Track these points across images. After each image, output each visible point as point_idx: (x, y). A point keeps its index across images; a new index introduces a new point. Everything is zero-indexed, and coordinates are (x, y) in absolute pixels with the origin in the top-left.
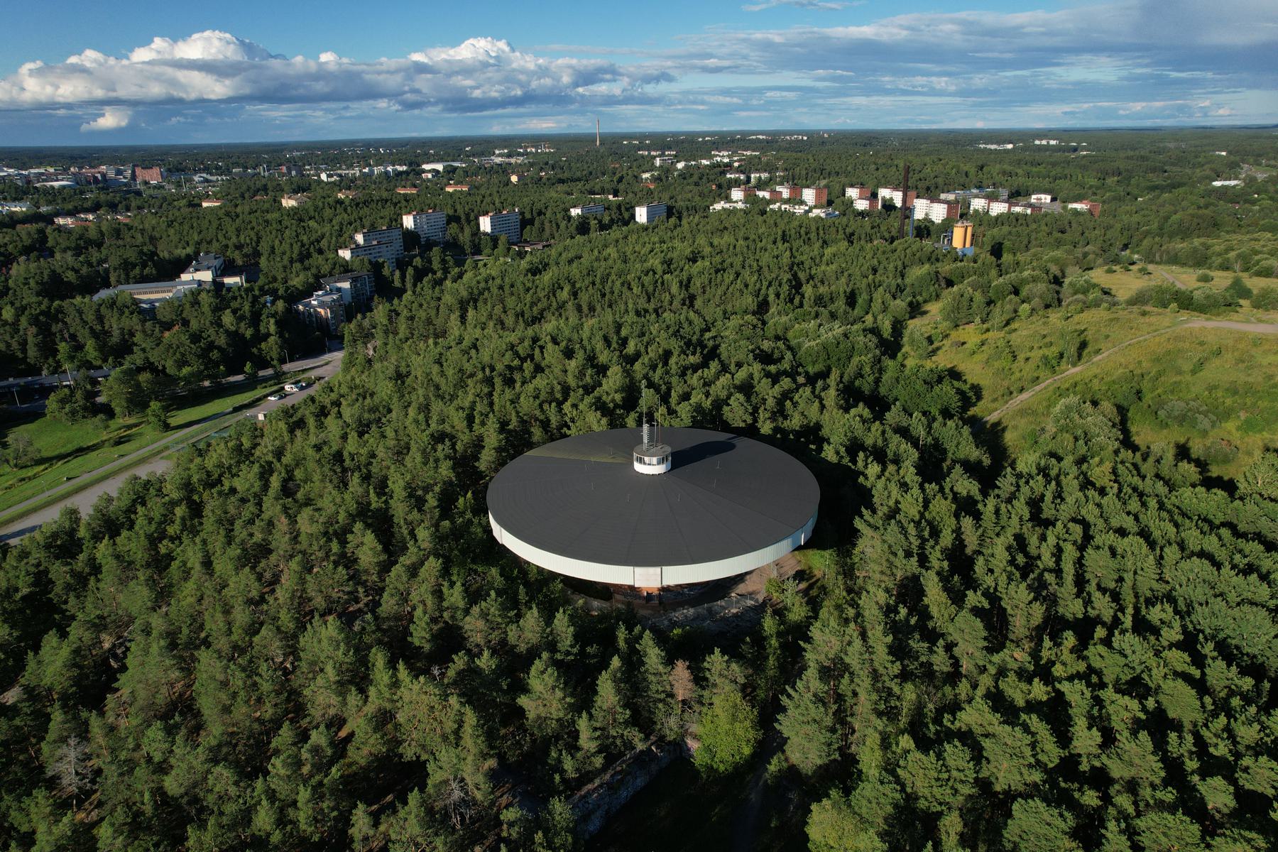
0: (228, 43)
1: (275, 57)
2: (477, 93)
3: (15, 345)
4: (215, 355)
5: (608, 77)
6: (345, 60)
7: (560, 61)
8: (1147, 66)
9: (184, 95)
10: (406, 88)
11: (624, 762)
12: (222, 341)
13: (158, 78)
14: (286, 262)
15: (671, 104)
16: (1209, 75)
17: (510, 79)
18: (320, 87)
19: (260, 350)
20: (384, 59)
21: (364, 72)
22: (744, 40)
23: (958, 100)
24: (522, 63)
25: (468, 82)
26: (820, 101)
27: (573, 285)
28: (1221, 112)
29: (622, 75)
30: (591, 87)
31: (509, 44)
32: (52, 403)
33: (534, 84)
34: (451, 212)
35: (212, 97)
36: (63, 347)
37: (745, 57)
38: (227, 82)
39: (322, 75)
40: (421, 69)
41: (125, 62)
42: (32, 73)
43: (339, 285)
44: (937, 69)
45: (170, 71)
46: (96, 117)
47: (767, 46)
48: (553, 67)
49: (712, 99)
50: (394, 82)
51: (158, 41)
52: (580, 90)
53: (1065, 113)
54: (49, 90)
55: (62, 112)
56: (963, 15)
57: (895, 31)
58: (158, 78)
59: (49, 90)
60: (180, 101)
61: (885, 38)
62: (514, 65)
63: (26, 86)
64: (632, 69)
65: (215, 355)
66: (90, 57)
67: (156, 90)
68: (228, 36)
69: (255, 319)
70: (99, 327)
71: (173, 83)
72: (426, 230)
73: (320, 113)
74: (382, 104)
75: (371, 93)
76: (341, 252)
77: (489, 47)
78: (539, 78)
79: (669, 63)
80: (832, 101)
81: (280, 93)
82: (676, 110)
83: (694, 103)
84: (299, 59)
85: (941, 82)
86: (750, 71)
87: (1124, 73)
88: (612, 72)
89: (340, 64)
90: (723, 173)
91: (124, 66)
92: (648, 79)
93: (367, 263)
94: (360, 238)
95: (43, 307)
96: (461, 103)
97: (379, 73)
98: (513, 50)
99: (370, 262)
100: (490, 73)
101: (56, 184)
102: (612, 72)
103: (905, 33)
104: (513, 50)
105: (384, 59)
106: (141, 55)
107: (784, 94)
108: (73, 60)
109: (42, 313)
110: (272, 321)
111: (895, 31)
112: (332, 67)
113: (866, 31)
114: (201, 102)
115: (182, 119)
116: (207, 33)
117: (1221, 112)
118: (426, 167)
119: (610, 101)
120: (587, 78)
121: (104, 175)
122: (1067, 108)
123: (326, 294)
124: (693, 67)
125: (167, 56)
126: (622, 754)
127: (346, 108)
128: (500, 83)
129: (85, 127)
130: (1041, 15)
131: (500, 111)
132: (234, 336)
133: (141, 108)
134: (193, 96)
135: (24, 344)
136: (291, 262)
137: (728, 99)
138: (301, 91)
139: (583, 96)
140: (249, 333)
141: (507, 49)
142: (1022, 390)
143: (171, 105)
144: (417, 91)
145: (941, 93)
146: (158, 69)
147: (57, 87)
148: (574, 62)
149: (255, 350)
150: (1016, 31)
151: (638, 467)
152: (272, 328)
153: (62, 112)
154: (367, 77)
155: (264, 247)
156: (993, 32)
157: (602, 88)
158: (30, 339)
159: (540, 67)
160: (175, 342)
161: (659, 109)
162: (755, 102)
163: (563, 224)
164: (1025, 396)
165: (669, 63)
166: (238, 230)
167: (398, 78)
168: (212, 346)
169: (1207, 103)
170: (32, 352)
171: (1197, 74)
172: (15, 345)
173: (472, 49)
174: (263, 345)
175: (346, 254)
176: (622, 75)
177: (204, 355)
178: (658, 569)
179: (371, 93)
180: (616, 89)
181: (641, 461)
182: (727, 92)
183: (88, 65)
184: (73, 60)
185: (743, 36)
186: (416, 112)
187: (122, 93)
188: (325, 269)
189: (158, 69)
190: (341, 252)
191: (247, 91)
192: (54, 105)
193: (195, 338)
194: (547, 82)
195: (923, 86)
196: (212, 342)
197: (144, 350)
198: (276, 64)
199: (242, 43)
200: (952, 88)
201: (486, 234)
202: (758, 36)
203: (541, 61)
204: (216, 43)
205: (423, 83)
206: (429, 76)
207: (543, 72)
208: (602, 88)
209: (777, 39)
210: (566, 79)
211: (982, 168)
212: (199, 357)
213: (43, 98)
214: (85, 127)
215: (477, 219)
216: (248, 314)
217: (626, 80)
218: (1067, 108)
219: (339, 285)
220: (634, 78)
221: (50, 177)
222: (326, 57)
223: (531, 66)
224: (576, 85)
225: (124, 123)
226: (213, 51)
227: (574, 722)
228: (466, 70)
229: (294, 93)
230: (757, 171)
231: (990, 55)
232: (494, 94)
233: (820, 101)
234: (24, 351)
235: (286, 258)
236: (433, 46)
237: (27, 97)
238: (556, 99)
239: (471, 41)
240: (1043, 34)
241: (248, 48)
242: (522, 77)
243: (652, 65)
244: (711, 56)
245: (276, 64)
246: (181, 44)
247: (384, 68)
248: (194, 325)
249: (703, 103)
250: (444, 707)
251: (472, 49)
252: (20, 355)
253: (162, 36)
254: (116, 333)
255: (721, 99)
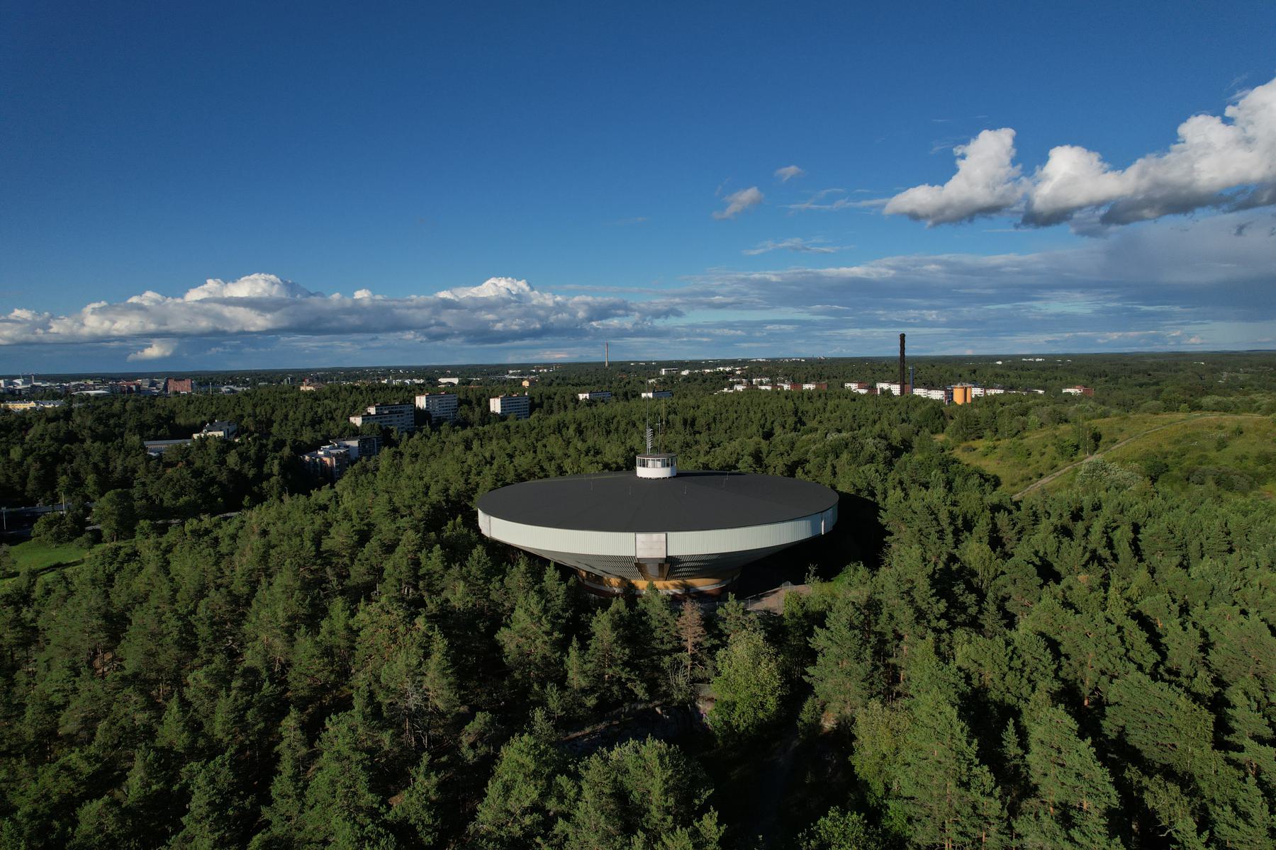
0: (273, 284)
1: (314, 295)
2: (499, 326)
3: (15, 478)
4: (214, 490)
5: (620, 312)
6: (379, 297)
7: (577, 299)
8: (1117, 300)
9: (227, 328)
10: (433, 322)
11: (617, 717)
12: (223, 477)
13: (206, 314)
14: (297, 426)
15: (679, 335)
16: (1177, 309)
17: (529, 314)
18: (354, 320)
19: (261, 488)
20: (414, 297)
21: (394, 306)
22: (744, 280)
23: (946, 330)
24: (541, 300)
25: (491, 317)
26: (818, 333)
27: (580, 424)
28: (1193, 340)
29: (632, 310)
30: (604, 322)
31: (529, 284)
32: (38, 527)
33: (552, 318)
34: (462, 397)
35: (253, 329)
36: (63, 480)
37: (745, 294)
38: (269, 316)
39: (357, 309)
40: (447, 304)
41: (179, 301)
42: (94, 312)
43: (348, 443)
44: (926, 303)
45: (217, 307)
46: (142, 348)
47: (765, 284)
48: (570, 303)
49: (718, 332)
50: (421, 316)
51: (210, 282)
52: (594, 324)
53: (1048, 342)
54: (107, 324)
55: (115, 344)
56: (945, 257)
57: (883, 270)
58: (206, 314)
59: (107, 324)
60: (224, 333)
61: (874, 276)
62: (534, 302)
63: (86, 322)
64: (642, 305)
65: (214, 490)
66: (149, 297)
67: (204, 324)
68: (273, 277)
69: (260, 461)
70: (102, 465)
71: (219, 317)
72: (437, 411)
73: (348, 344)
74: (409, 335)
75: (399, 326)
76: (352, 419)
77: (509, 286)
78: (557, 313)
79: (677, 300)
80: (828, 333)
81: (312, 326)
82: (682, 342)
83: (702, 335)
84: (336, 296)
85: (932, 315)
86: (752, 307)
87: (1098, 307)
88: (626, 309)
89: (373, 300)
90: (727, 378)
91: (177, 304)
92: (657, 314)
93: (376, 428)
94: (372, 410)
95: (52, 449)
96: (484, 335)
97: (409, 308)
98: (532, 289)
99: (380, 427)
100: (512, 309)
101: (92, 393)
102: (626, 309)
103: (892, 272)
104: (532, 289)
105: (414, 297)
106: (194, 295)
107: (783, 327)
108: (134, 300)
109: (50, 454)
110: (276, 462)
111: (883, 270)
112: (367, 303)
113: (857, 271)
114: (243, 334)
115: (220, 349)
116: (255, 276)
117: (1193, 340)
118: (442, 380)
119: (622, 333)
120: (602, 313)
121: (138, 387)
122: (1049, 337)
123: (334, 448)
124: (700, 304)
125: (218, 296)
126: (619, 704)
127: (372, 339)
128: (519, 317)
129: (132, 357)
130: (1013, 257)
131: (518, 343)
132: (236, 476)
133: (186, 340)
134: (235, 328)
135: (24, 478)
136: (303, 425)
137: (732, 332)
138: (335, 324)
139: (596, 329)
140: (251, 473)
141: (527, 289)
142: (1041, 475)
143: (216, 336)
144: (443, 324)
145: (933, 324)
146: (207, 306)
147: (114, 322)
148: (589, 299)
149: (256, 489)
150: (995, 270)
151: (642, 472)
152: (276, 469)
153: (115, 344)
154: (397, 311)
155: (278, 417)
156: (972, 271)
157: (614, 322)
158: (32, 473)
159: (557, 303)
160: (176, 476)
161: (664, 341)
162: (758, 334)
163: (571, 405)
164: (1044, 480)
165: (677, 300)
166: (255, 406)
167: (426, 313)
168: (212, 481)
169: (1178, 333)
170: (31, 486)
171: (1166, 308)
172: (15, 478)
173: (493, 288)
174: (265, 484)
175: (357, 421)
176: (632, 310)
177: (203, 489)
178: (663, 535)
179: (399, 326)
180: (628, 323)
181: (644, 465)
182: (730, 325)
183: (146, 303)
184: (134, 300)
185: (743, 276)
186: (439, 343)
187: (172, 326)
188: (336, 431)
189: (207, 306)
190: (352, 419)
191: (285, 323)
192: (108, 338)
193: (197, 473)
194: (565, 316)
195: (915, 318)
196: (214, 478)
197: (144, 484)
198: (316, 301)
199: (285, 283)
200: (943, 320)
201: (495, 414)
202: (757, 276)
203: (559, 298)
204: (262, 283)
205: (448, 317)
206: (454, 311)
207: (559, 308)
208: (614, 322)
209: (774, 279)
210: (581, 314)
211: (975, 372)
212: (198, 491)
213: (99, 332)
214: (132, 357)
215: (488, 402)
216: (253, 457)
217: (637, 314)
218: (1049, 337)
219: (348, 443)
220: (644, 313)
221: (88, 387)
222: (361, 294)
223: (550, 303)
224: (591, 320)
225: (168, 354)
226: (259, 290)
227: (562, 662)
228: (488, 305)
229: (328, 325)
230: (758, 376)
231: (973, 291)
232: (516, 328)
233: (818, 333)
234: (24, 484)
235: (297, 423)
236: (457, 286)
237: (85, 331)
238: (571, 331)
239: (493, 280)
240: (1019, 273)
241: (291, 287)
242: (541, 313)
243: (660, 302)
244: (714, 294)
245: (316, 301)
246: (230, 285)
247: (414, 303)
248: (198, 464)
249: (708, 335)
250: (408, 630)
251: (493, 288)
252: (18, 488)
253: (214, 278)
254: (120, 468)
255: (727, 332)
